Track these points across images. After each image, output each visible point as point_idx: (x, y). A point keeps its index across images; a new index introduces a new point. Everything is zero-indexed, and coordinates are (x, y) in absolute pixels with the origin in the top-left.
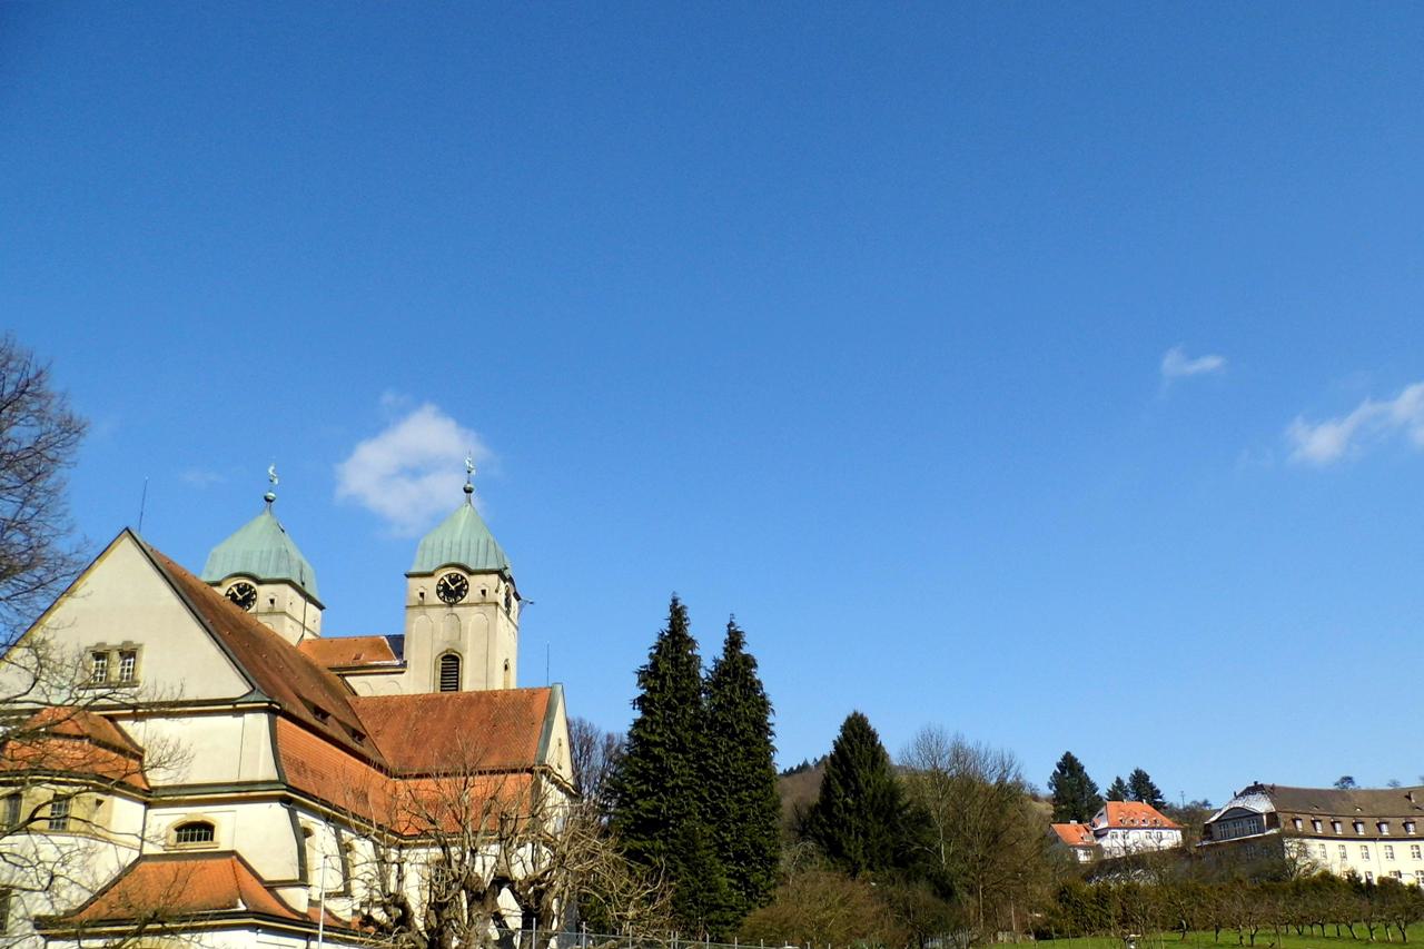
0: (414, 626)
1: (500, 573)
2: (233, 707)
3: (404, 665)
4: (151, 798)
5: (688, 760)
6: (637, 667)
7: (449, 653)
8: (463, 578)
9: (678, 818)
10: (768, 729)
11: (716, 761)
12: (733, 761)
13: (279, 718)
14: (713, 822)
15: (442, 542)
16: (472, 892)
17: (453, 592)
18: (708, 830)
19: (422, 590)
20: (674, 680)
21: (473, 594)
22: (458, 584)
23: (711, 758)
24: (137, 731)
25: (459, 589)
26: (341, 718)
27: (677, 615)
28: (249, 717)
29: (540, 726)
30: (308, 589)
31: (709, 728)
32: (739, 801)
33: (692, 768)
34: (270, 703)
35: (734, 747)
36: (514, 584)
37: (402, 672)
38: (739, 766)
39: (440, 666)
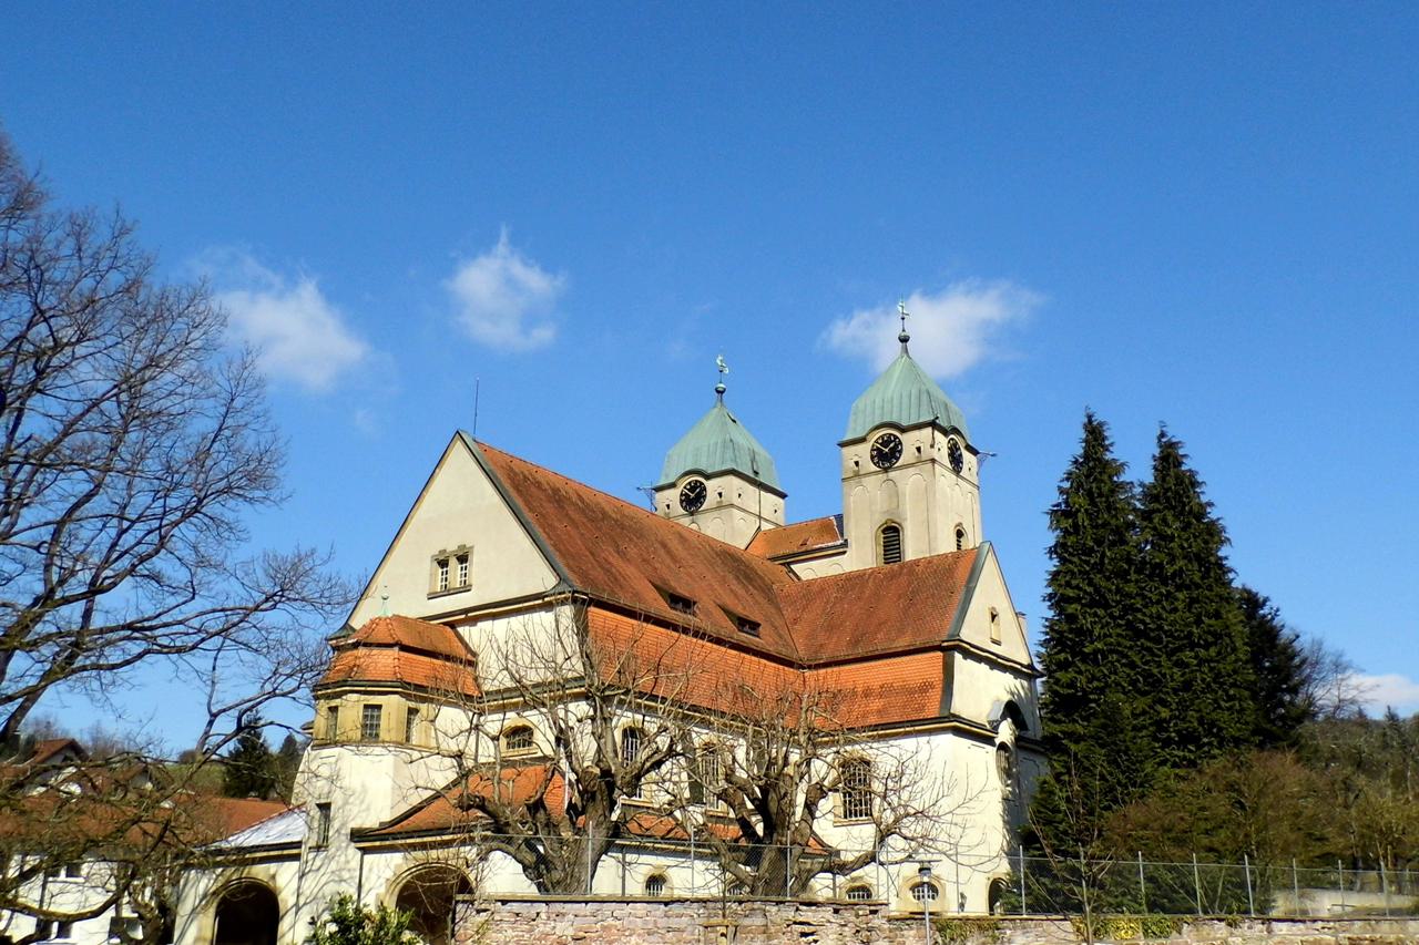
1: (933, 425)
3: (845, 544)
5: (1111, 616)
6: (1048, 507)
7: (890, 524)
8: (896, 437)
9: (1101, 691)
11: (1144, 614)
13: (592, 609)
14: (1144, 694)
15: (874, 402)
17: (887, 455)
18: (1141, 703)
19: (856, 459)
21: (908, 455)
22: (892, 445)
23: (1139, 610)
24: (474, 634)
26: (739, 610)
27: (1095, 435)
29: (959, 596)
30: (761, 479)
31: (1138, 572)
32: (1181, 664)
33: (1120, 626)
37: (844, 552)
38: (1177, 616)
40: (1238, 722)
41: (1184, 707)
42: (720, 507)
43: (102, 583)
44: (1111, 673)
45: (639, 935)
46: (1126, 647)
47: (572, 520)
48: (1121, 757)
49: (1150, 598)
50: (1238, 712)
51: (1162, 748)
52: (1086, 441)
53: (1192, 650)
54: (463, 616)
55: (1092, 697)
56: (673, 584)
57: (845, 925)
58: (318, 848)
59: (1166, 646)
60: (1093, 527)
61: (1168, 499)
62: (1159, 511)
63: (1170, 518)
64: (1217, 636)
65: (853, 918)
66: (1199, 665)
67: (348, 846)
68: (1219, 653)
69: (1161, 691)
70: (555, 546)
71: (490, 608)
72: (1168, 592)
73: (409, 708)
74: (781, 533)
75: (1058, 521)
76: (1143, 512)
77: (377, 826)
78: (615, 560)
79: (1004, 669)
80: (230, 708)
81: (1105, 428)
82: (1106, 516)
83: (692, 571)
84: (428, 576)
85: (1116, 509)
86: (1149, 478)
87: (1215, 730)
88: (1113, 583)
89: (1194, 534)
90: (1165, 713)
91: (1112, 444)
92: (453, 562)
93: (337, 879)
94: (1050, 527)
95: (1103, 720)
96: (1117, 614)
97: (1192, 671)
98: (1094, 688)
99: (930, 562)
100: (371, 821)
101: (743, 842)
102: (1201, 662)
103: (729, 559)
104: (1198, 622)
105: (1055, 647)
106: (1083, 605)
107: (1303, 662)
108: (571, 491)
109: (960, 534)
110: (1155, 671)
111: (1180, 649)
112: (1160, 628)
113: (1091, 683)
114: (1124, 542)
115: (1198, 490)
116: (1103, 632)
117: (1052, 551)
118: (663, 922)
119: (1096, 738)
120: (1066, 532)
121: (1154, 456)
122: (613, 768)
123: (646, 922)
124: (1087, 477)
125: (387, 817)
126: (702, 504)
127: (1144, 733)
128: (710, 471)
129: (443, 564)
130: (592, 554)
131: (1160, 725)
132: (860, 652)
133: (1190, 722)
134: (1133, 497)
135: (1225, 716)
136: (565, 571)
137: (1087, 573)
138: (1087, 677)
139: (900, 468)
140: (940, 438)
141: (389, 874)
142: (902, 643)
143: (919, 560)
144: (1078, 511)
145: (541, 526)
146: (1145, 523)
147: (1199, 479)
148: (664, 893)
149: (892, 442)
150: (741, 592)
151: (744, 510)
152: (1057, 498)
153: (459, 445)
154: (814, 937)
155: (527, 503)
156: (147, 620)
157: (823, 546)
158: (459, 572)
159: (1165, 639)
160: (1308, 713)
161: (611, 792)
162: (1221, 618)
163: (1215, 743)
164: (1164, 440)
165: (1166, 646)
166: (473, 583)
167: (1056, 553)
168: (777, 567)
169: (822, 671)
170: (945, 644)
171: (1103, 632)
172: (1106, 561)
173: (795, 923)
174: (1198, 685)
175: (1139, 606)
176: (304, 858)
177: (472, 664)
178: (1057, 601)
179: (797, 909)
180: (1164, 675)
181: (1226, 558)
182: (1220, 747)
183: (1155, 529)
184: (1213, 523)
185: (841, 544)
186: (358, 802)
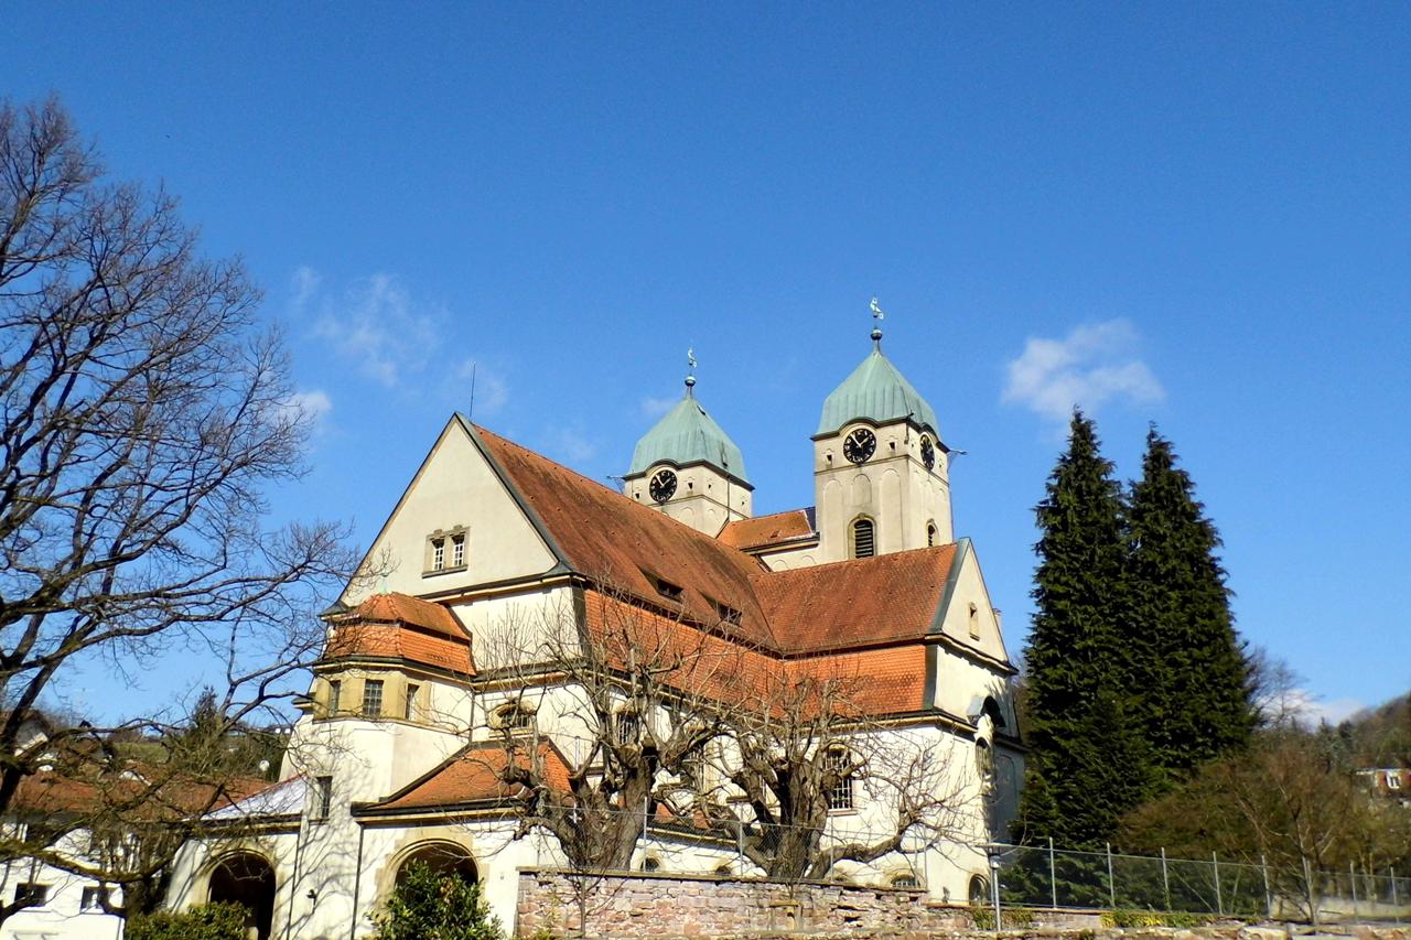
0: (824, 492)
1: (908, 421)
2: (538, 584)
3: (817, 537)
4: (476, 682)
6: (1035, 503)
7: (862, 519)
8: (870, 433)
9: (1093, 688)
10: (1214, 566)
11: (1136, 612)
12: (1163, 611)
14: (1137, 692)
16: (628, 768)
17: (860, 450)
18: (1134, 701)
19: (829, 453)
20: (1079, 514)
21: (882, 449)
22: (865, 440)
25: (866, 446)
26: (719, 598)
28: (556, 592)
29: (940, 590)
30: (730, 471)
31: (1130, 570)
32: (1173, 663)
33: (1109, 623)
34: (571, 574)
35: (1161, 592)
36: (935, 434)
37: (816, 545)
38: (1171, 616)
39: (854, 534)
40: (1232, 723)
41: (1178, 706)
42: (690, 497)
43: (122, 551)
44: (1101, 670)
45: (692, 914)
46: (1117, 645)
47: (564, 505)
48: (1115, 755)
49: (1143, 597)
50: (1233, 713)
51: (1155, 747)
52: (1074, 440)
53: (1185, 649)
54: (459, 596)
55: (1082, 694)
56: (659, 570)
57: (887, 912)
58: (320, 822)
59: (1160, 645)
60: (1081, 524)
61: (1159, 499)
62: (1150, 510)
63: (1162, 518)
64: (1212, 637)
65: (894, 905)
66: (1193, 664)
67: (350, 820)
68: (1213, 654)
69: (1154, 690)
70: (551, 528)
71: (485, 588)
72: (1161, 591)
73: (410, 685)
74: (747, 525)
75: (1046, 518)
76: (1134, 511)
77: (377, 801)
78: (604, 543)
79: (982, 664)
80: (251, 677)
81: (1092, 427)
82: (1095, 514)
83: (673, 558)
84: (423, 557)
85: (1106, 507)
86: (1140, 478)
87: (1210, 731)
88: (1103, 581)
89: (1186, 535)
90: (1159, 712)
91: (1099, 444)
92: (449, 542)
93: (340, 851)
94: (1037, 524)
95: (1097, 718)
96: (1108, 612)
97: (1187, 671)
98: (1085, 685)
99: (907, 556)
100: (371, 796)
101: (757, 826)
102: (1195, 662)
103: (704, 548)
104: (1192, 622)
105: (1043, 642)
106: (1073, 602)
107: (1252, 670)
108: (560, 477)
109: (931, 530)
110: (1149, 669)
111: (1173, 648)
112: (1153, 626)
113: (1082, 679)
114: (1113, 540)
115: (1188, 490)
116: (1094, 628)
117: (1040, 547)
118: (714, 901)
119: (1089, 734)
120: (1054, 529)
121: (1144, 456)
122: (658, 745)
123: (698, 901)
124: (1076, 475)
125: (387, 793)
126: (672, 494)
127: (1137, 731)
128: (680, 462)
129: (438, 543)
130: (585, 538)
131: (1154, 724)
132: (840, 643)
133: (1184, 721)
134: (1121, 496)
135: (1219, 717)
136: (563, 554)
137: (1077, 570)
138: (1078, 674)
139: (873, 463)
140: (915, 436)
141: (391, 849)
142: (883, 636)
143: (897, 554)
144: (1067, 508)
145: (537, 509)
146: (1136, 523)
147: (1192, 479)
148: (656, 872)
149: (865, 437)
150: (719, 581)
151: (714, 501)
152: (1045, 495)
153: (456, 427)
154: (858, 922)
155: (523, 486)
156: (179, 586)
157: (795, 538)
158: (454, 552)
159: (1158, 638)
160: (1258, 720)
161: (653, 769)
162: (1214, 618)
163: (1210, 744)
164: (1154, 440)
165: (1160, 645)
166: (469, 562)
167: (1043, 549)
168: (749, 559)
169: (840, 657)
170: (928, 638)
171: (1094, 628)
172: (1097, 559)
173: (840, 907)
174: (1192, 684)
175: (1130, 604)
176: (302, 831)
177: (468, 643)
178: (1046, 597)
179: (841, 894)
180: (1157, 674)
181: (1219, 559)
182: (1214, 747)
183: (1146, 528)
184: (1204, 523)
185: (813, 537)
186: (361, 776)
